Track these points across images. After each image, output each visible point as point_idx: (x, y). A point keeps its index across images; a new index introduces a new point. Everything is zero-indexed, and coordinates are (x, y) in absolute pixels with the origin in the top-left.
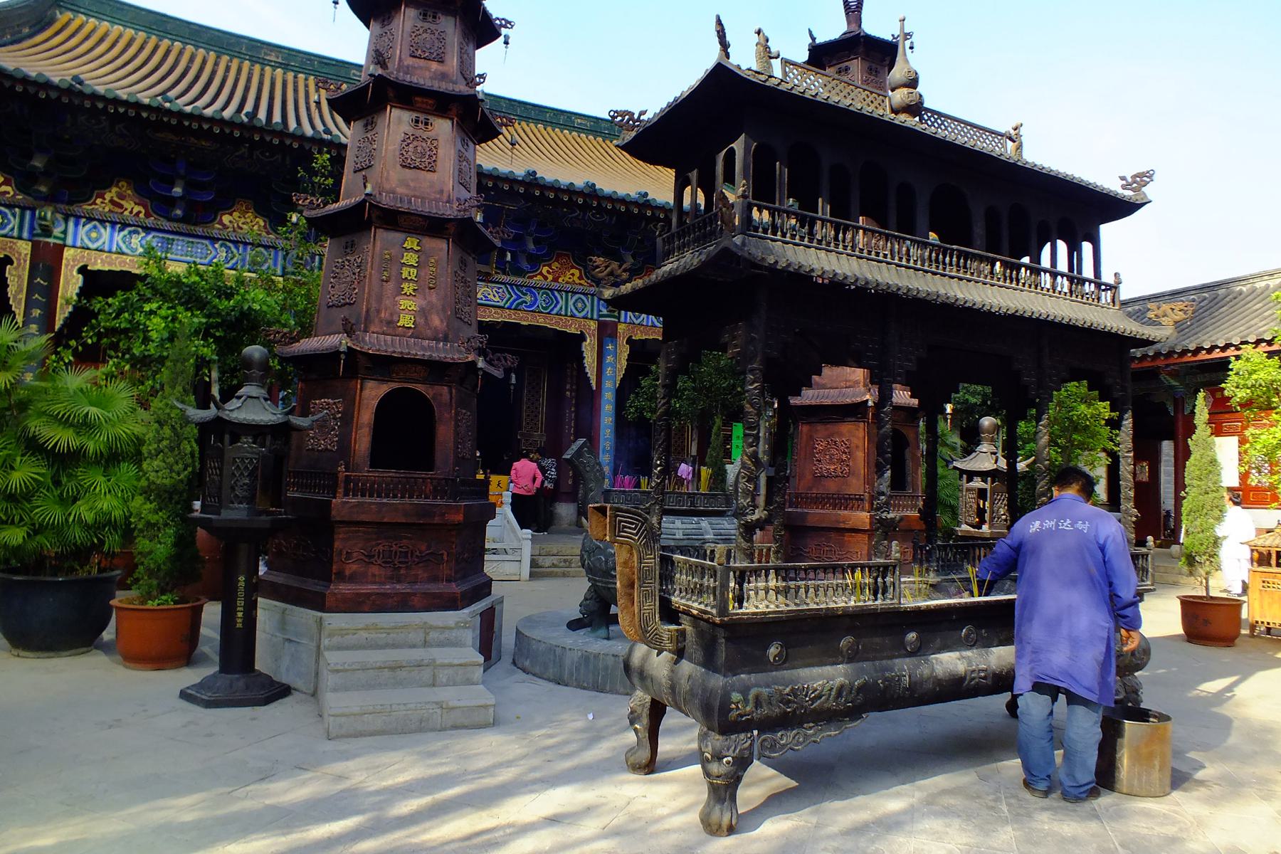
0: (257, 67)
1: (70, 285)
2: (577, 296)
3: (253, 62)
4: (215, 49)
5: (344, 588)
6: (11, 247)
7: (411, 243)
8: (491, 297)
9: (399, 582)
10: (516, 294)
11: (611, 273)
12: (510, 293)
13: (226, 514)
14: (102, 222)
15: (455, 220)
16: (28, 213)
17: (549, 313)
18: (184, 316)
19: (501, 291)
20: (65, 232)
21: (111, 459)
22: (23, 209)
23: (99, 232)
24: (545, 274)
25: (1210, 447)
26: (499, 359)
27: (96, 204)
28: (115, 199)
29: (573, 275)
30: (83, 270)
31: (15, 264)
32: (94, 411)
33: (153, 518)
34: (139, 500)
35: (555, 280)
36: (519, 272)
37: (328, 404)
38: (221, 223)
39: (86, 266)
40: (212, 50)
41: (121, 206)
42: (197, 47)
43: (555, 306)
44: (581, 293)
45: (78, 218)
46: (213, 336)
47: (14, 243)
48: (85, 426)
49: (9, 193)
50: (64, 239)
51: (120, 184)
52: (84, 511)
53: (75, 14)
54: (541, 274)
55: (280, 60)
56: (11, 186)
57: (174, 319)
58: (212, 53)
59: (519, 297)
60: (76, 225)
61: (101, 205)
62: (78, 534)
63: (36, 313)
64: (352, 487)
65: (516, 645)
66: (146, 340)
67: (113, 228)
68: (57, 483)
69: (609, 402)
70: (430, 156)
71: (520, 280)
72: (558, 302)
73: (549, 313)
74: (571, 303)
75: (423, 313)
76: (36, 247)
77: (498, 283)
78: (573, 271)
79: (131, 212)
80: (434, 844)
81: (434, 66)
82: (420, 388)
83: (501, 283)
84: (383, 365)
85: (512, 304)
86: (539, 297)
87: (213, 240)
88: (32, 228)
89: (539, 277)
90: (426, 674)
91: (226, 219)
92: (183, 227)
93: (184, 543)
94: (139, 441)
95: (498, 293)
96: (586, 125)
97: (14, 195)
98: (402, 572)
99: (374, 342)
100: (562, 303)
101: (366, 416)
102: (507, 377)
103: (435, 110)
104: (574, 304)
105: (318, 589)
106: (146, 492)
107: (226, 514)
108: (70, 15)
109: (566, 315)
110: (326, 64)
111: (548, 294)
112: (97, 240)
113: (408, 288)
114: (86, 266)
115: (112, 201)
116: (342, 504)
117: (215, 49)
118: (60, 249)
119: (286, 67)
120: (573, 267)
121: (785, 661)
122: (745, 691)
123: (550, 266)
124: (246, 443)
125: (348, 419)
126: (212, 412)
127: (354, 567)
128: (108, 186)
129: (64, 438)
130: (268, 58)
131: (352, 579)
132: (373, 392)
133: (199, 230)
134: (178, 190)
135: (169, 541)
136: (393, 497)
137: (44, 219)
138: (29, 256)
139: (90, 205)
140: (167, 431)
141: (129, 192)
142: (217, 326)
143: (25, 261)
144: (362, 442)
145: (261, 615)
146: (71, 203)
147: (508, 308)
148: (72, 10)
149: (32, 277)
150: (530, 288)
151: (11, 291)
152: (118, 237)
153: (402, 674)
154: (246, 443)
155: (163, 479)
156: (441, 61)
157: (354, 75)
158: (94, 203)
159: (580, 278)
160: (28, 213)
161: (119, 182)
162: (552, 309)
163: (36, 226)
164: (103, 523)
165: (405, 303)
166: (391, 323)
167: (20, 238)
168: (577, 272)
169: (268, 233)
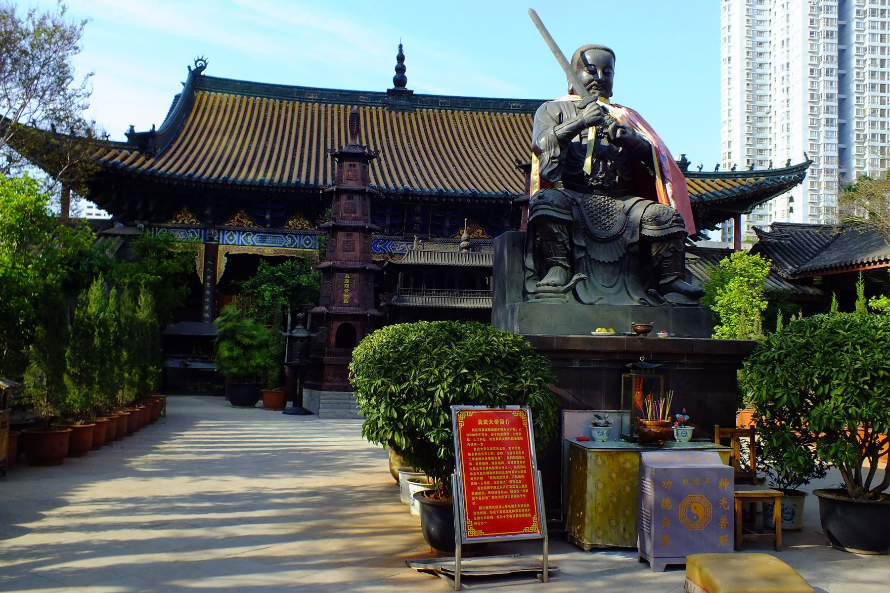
0: (304, 104)
1: (222, 263)
3: (301, 102)
5: (328, 384)
7: (347, 276)
13: (293, 362)
14: (234, 231)
16: (203, 231)
18: (276, 288)
20: (219, 238)
21: (259, 347)
22: (201, 229)
23: (233, 236)
29: (478, 233)
30: (227, 255)
32: (254, 332)
33: (273, 365)
34: (268, 359)
38: (288, 225)
41: (242, 222)
42: (269, 98)
45: (224, 231)
46: (288, 295)
48: (252, 337)
50: (218, 241)
52: (253, 363)
55: (317, 98)
57: (273, 290)
58: (277, 100)
60: (223, 234)
61: (234, 223)
62: (251, 370)
63: (209, 277)
64: (330, 354)
66: (264, 300)
67: (239, 234)
68: (245, 354)
75: (351, 299)
76: (207, 246)
78: (477, 231)
81: (353, 215)
82: (350, 322)
84: (338, 317)
87: (285, 234)
88: (205, 238)
90: (348, 406)
91: (290, 223)
92: (271, 230)
93: (282, 371)
94: (267, 341)
96: (519, 107)
99: (336, 309)
101: (334, 332)
106: (270, 357)
107: (293, 362)
108: (201, 92)
110: (344, 95)
112: (232, 240)
113: (346, 290)
115: (238, 220)
116: (327, 359)
118: (217, 246)
119: (320, 101)
120: (478, 228)
124: (299, 342)
125: (329, 333)
126: (288, 334)
128: (235, 214)
129: (247, 341)
131: (330, 381)
132: (337, 325)
133: (278, 231)
134: (268, 216)
135: (278, 371)
137: (211, 234)
140: (276, 338)
142: (289, 290)
144: (333, 340)
145: (304, 393)
146: (220, 224)
148: (202, 90)
152: (242, 238)
153: (341, 405)
154: (299, 342)
155: (275, 353)
157: (362, 99)
159: (483, 234)
160: (203, 231)
164: (258, 366)
165: (345, 296)
166: (342, 302)
168: (480, 231)
169: (311, 228)
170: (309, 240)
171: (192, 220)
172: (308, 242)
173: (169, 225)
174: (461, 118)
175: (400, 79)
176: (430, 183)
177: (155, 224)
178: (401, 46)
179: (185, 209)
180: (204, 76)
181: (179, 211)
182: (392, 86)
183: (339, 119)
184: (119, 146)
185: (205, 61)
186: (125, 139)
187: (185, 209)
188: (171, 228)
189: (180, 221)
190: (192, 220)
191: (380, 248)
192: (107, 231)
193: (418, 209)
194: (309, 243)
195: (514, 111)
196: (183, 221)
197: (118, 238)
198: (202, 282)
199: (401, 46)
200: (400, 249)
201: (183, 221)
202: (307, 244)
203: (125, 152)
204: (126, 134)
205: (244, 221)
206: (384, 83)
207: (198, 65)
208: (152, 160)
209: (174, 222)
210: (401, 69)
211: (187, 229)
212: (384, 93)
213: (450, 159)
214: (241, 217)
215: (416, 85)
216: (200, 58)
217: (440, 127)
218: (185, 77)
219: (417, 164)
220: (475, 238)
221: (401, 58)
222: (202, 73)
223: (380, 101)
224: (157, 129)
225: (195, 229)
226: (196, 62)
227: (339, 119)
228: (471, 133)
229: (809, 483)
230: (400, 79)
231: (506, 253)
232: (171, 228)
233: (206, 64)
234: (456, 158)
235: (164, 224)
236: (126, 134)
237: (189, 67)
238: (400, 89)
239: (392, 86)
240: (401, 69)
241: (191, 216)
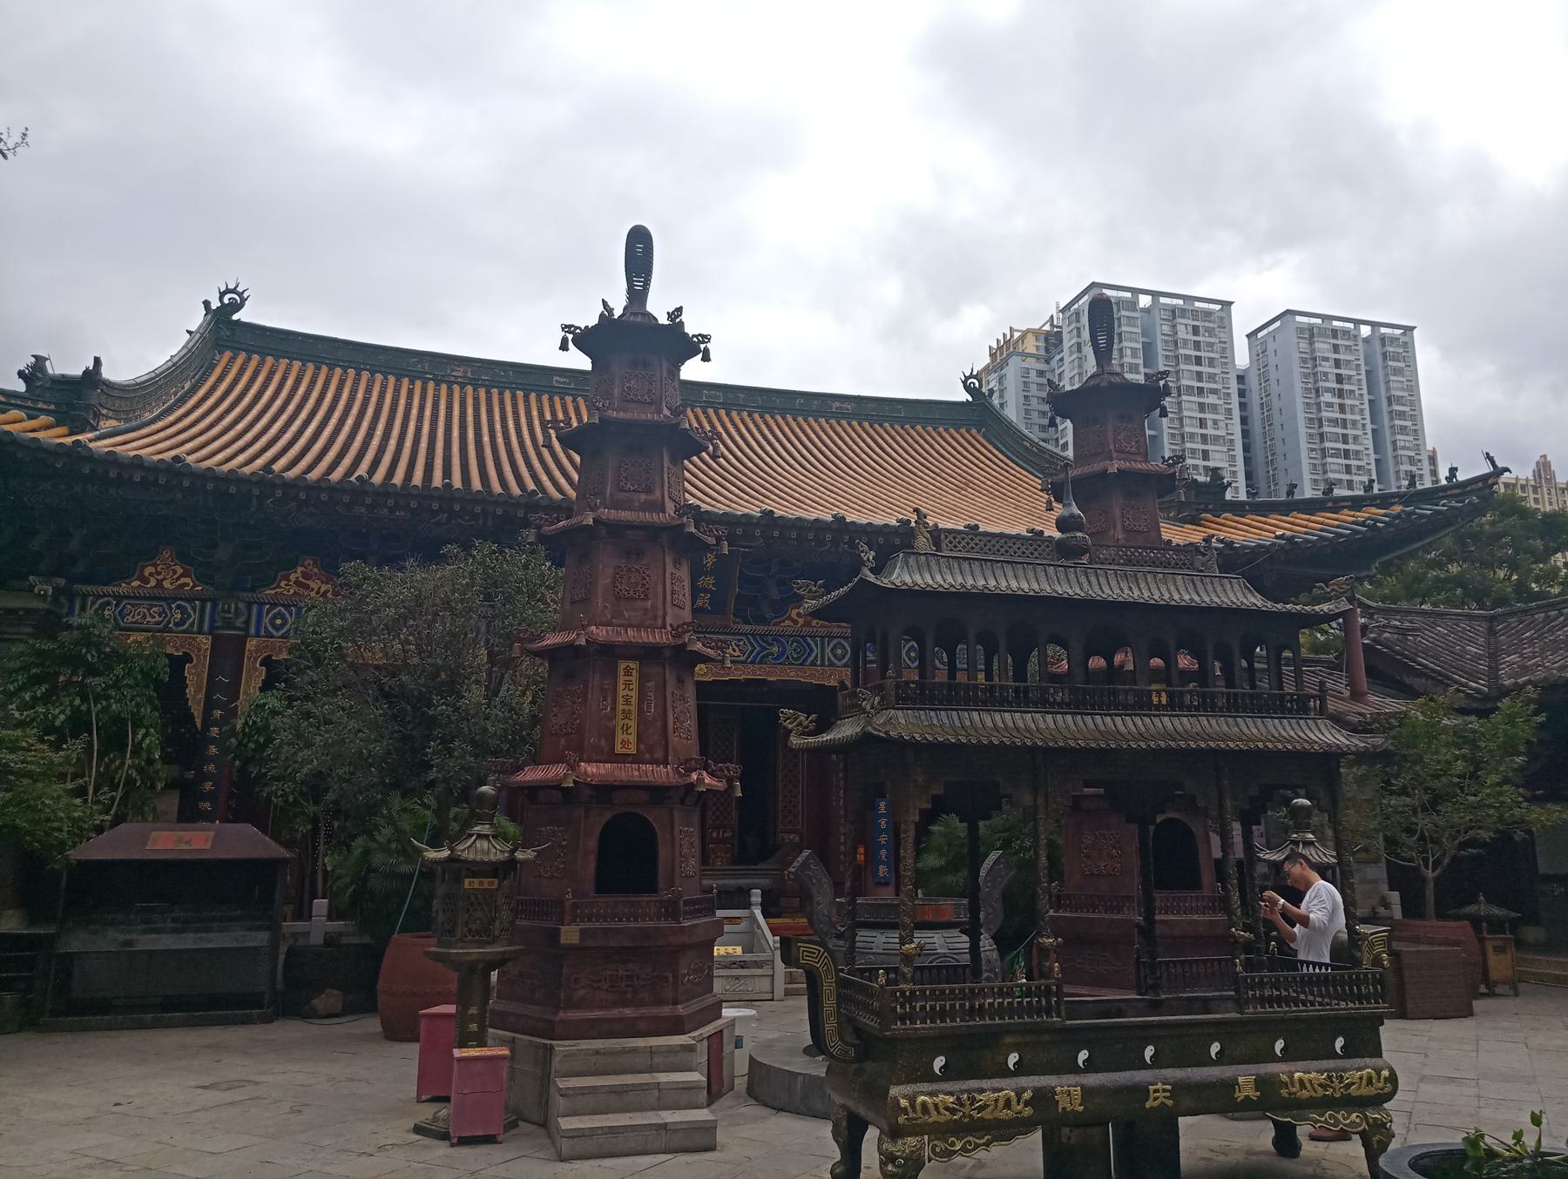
2: (835, 641)
4: (395, 371)
6: (190, 644)
9: (625, 1006)
10: (760, 645)
11: (800, 724)
12: (752, 645)
15: (669, 647)
16: (209, 605)
17: (801, 664)
19: (741, 643)
22: (203, 601)
24: (795, 618)
26: (721, 770)
27: (281, 587)
28: (301, 579)
31: (195, 661)
36: (761, 620)
37: (554, 832)
39: (270, 656)
40: (390, 373)
41: (307, 587)
43: (809, 655)
44: (840, 637)
47: (194, 639)
49: (188, 585)
50: (247, 629)
51: (306, 563)
53: (237, 351)
56: (190, 577)
59: (764, 649)
70: (643, 585)
71: (762, 629)
72: (811, 651)
73: (801, 664)
74: (828, 650)
77: (738, 634)
79: (318, 593)
81: (643, 497)
83: (741, 634)
85: (755, 657)
86: (788, 647)
88: (212, 620)
89: (788, 623)
95: (738, 646)
97: (195, 586)
98: (629, 996)
102: (731, 787)
104: (832, 651)
105: (1432, 883)
109: (823, 665)
111: (798, 642)
114: (270, 656)
115: (297, 583)
117: (395, 371)
118: (242, 641)
122: (912, 1100)
127: (582, 992)
130: (454, 374)
131: (578, 1006)
132: (600, 819)
136: (619, 921)
138: (209, 652)
139: (275, 589)
141: (316, 570)
143: (205, 657)
146: (253, 590)
147: (751, 663)
150: (777, 639)
151: (190, 691)
156: (649, 491)
158: (279, 586)
160: (209, 605)
161: (305, 560)
162: (805, 660)
163: (217, 617)
167: (200, 632)
171: (183, 580)
179: (166, 554)
181: (150, 556)
187: (166, 554)
188: (128, 597)
189: (153, 583)
190: (183, 580)
191: (771, 645)
194: (282, 626)
196: (159, 584)
201: (159, 584)
202: (277, 628)
205: (312, 584)
209: (136, 583)
211: (169, 599)
214: (305, 575)
216: (231, 286)
217: (922, 442)
218: (197, 319)
226: (222, 295)
229: (1434, 451)
231: (238, 633)
232: (128, 597)
233: (243, 301)
234: (755, 439)
235: (109, 589)
237: (207, 304)
241: (180, 571)
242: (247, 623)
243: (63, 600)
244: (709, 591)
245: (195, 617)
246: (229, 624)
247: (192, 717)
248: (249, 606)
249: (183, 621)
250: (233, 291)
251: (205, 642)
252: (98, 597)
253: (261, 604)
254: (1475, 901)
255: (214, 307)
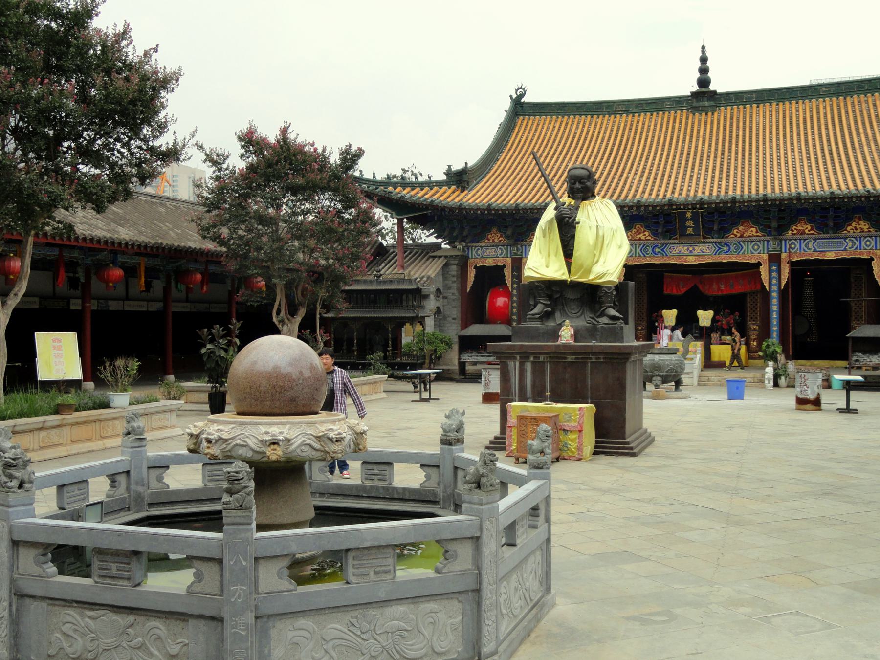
8: (705, 251)
24: (736, 233)
25: (198, 462)
35: (742, 236)
50: (781, 251)
54: (733, 234)
59: (720, 249)
63: (515, 286)
65: (43, 270)
69: (774, 298)
78: (752, 229)
80: (527, 251)
86: (731, 247)
88: (511, 253)
96: (830, 91)
100: (745, 248)
103: (629, 354)
120: (752, 227)
121: (398, 369)
123: (738, 229)
149: (513, 271)
151: (506, 278)
157: (666, 105)
159: (757, 232)
160: (766, 242)
170: (869, 241)
172: (868, 243)
173: (482, 244)
174: (761, 114)
175: (704, 82)
176: (542, 190)
177: (473, 244)
178: (703, 48)
179: (495, 230)
180: (524, 103)
182: (696, 88)
183: (497, 178)
184: (440, 184)
185: (524, 89)
186: (444, 178)
187: (495, 230)
192: (434, 254)
193: (689, 215)
195: (824, 96)
196: (493, 240)
197: (443, 258)
198: (510, 289)
199: (703, 48)
200: (677, 251)
201: (493, 240)
203: (445, 188)
204: (444, 173)
206: (688, 86)
207: (518, 94)
208: (466, 192)
210: (704, 71)
211: (497, 246)
212: (688, 96)
213: (736, 160)
215: (719, 84)
218: (507, 105)
219: (736, 160)
220: (749, 236)
221: (704, 60)
222: (522, 100)
223: (685, 105)
224: (469, 166)
225: (503, 246)
226: (517, 91)
227: (497, 178)
228: (724, 138)
230: (704, 82)
233: (525, 92)
236: (444, 173)
237: (511, 96)
238: (704, 90)
239: (696, 88)
240: (704, 71)
242: (781, 248)
243: (466, 249)
244: (691, 227)
245: (505, 252)
246: (516, 254)
247: (765, 286)
248: (781, 241)
249: (502, 253)
250: (521, 88)
251: (509, 260)
252: (805, 240)
253: (785, 240)
254: (258, 306)
255: (514, 98)
